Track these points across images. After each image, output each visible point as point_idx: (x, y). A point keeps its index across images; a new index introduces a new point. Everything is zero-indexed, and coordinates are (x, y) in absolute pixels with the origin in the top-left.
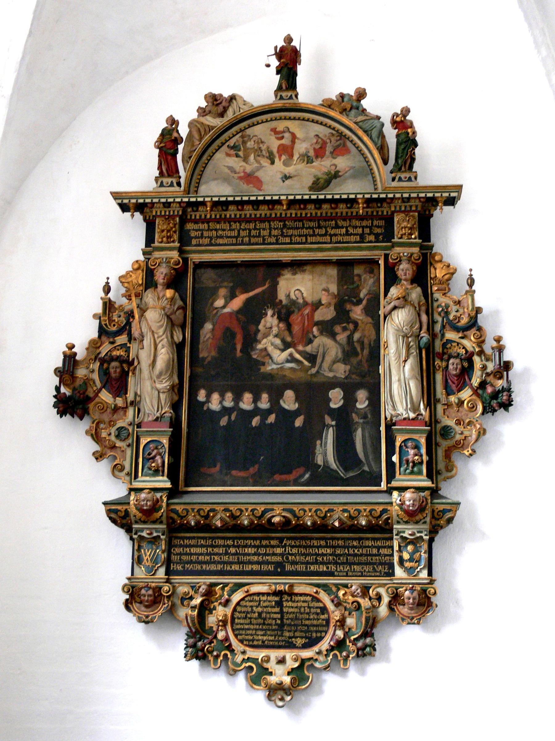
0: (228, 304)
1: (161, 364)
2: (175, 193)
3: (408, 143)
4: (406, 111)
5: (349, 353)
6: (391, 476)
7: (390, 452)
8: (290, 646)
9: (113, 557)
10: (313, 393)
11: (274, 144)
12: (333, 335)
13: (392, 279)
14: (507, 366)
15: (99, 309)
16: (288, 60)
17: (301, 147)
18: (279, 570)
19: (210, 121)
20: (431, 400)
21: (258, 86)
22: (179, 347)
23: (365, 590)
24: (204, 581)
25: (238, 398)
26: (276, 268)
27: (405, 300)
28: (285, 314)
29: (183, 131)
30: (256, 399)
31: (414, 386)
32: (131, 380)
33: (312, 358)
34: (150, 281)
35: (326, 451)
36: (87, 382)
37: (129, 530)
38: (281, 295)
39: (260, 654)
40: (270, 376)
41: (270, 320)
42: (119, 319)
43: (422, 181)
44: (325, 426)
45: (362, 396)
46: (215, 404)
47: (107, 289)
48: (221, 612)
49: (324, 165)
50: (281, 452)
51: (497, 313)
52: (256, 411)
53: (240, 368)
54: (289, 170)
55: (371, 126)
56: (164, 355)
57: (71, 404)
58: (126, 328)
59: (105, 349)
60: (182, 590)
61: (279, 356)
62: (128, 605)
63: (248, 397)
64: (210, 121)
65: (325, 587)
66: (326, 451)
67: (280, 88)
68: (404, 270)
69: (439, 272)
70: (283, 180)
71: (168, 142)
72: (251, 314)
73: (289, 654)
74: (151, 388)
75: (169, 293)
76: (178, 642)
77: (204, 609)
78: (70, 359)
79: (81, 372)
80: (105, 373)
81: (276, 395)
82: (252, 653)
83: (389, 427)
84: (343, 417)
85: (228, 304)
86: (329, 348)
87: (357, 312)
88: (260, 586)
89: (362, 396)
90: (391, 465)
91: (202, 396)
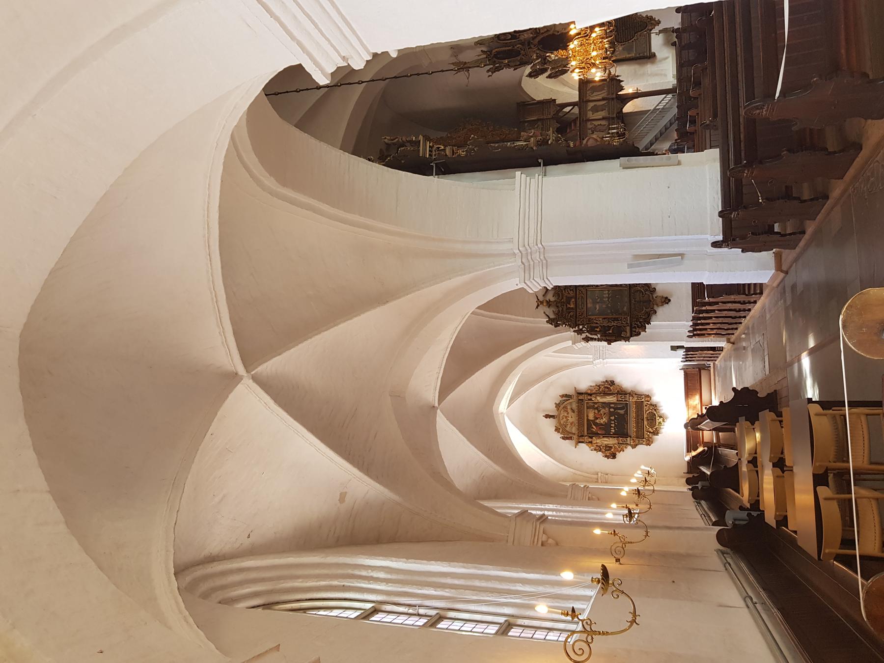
2: (575, 437)
3: (566, 396)
10: (611, 414)
16: (547, 416)
34: (591, 442)
35: (622, 412)
41: (597, 421)
49: (569, 411)
57: (614, 457)
66: (622, 412)
70: (572, 418)
71: (564, 438)
72: (596, 424)
76: (656, 437)
86: (602, 411)
88: (646, 423)
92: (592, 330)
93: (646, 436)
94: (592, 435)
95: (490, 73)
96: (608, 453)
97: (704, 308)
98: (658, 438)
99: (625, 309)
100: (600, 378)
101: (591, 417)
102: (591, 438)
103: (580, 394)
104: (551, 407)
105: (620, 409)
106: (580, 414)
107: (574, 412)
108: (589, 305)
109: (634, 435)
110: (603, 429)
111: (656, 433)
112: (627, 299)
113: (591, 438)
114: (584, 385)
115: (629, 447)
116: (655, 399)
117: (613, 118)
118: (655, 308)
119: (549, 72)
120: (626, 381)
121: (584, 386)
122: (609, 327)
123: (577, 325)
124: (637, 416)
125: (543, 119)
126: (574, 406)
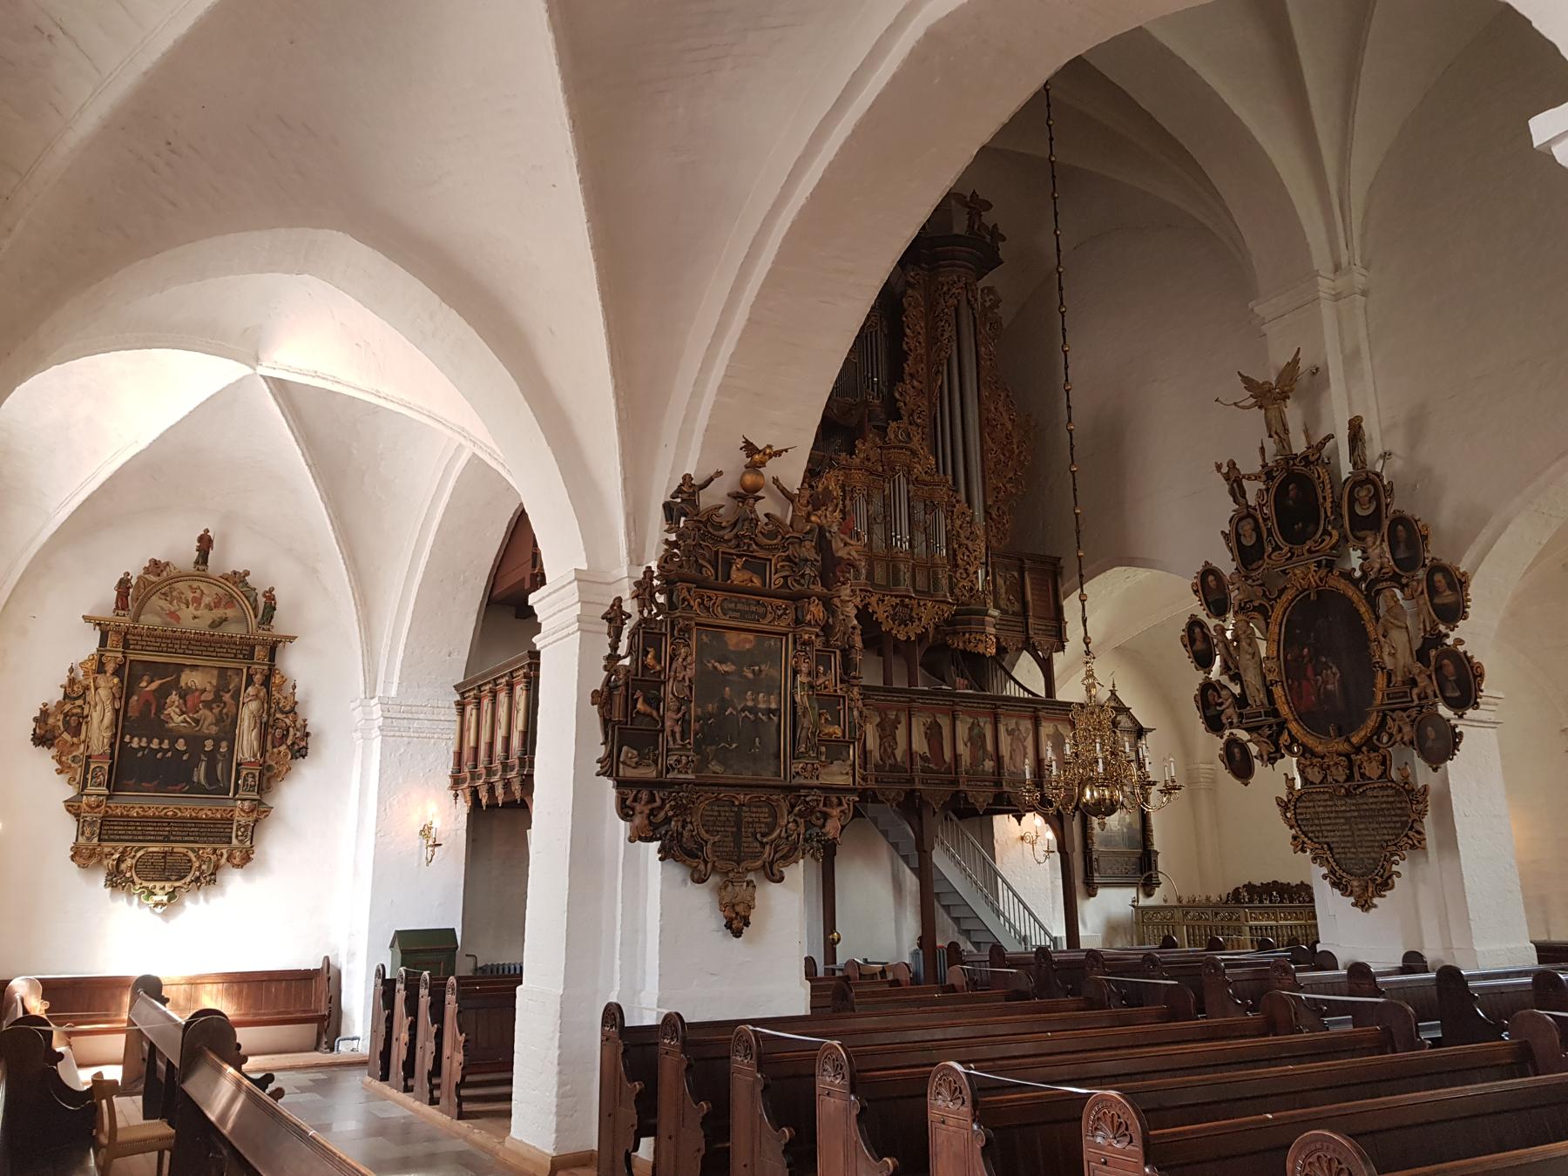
0: (149, 686)
1: (107, 721)
2: (126, 621)
3: (271, 608)
4: (272, 589)
5: (219, 720)
6: (236, 793)
7: (237, 779)
8: (168, 880)
9: (66, 831)
10: (195, 741)
11: (190, 596)
12: (211, 709)
13: (250, 682)
14: (307, 735)
15: (65, 681)
16: (205, 543)
17: (206, 600)
18: (167, 840)
19: (152, 578)
20: (263, 751)
21: (183, 552)
22: (117, 711)
23: (215, 851)
24: (121, 846)
25: (150, 742)
26: (180, 668)
27: (257, 696)
28: (183, 695)
29: (134, 582)
30: (161, 743)
31: (255, 744)
32: (84, 727)
33: (197, 721)
34: (101, 669)
35: (200, 774)
36: (55, 727)
37: (77, 816)
38: (182, 684)
39: (151, 885)
40: (171, 730)
41: (174, 697)
42: (78, 689)
43: (275, 632)
44: (201, 760)
45: (224, 744)
46: (135, 744)
47: (71, 670)
48: (129, 862)
49: (219, 613)
50: (170, 773)
51: (317, 735)
52: (161, 749)
53: (151, 722)
54: (197, 613)
55: (250, 593)
56: (109, 715)
57: (42, 738)
58: (83, 696)
59: (67, 707)
60: (107, 850)
61: (177, 719)
62: (73, 858)
63: (156, 741)
64: (152, 578)
65: (192, 850)
66: (200, 774)
67: (197, 563)
68: (258, 678)
69: (277, 680)
70: (194, 619)
71: (124, 585)
72: (163, 693)
73: (168, 885)
74: (99, 730)
75: (116, 680)
76: (101, 879)
77: (120, 861)
78: (45, 713)
79: (51, 721)
80: (66, 723)
81: (173, 742)
82: (145, 884)
83: (239, 765)
84: (212, 756)
85: (149, 686)
86: (207, 716)
87: (227, 697)
88: (154, 848)
89: (224, 744)
90: (237, 784)
91: (127, 739)
92: (647, 636)
93: (107, 847)
94: (128, 675)
95: (1224, 470)
96: (56, 721)
97: (424, 992)
98: (97, 884)
99: (715, 767)
100: (317, 715)
101: (190, 679)
102: (116, 673)
103: (273, 649)
104: (235, 556)
105: (211, 772)
106: (202, 645)
107: (215, 624)
108: (732, 639)
109: (118, 807)
110: (144, 714)
111: (117, 880)
112: (747, 776)
113: (116, 673)
114: (299, 667)
115: (70, 792)
116: (235, 883)
117: (998, 784)
118: (714, 880)
119: (1212, 623)
120: (297, 795)
121: (297, 666)
122: (654, 702)
123: (669, 586)
124: (181, 823)
125: (1026, 617)
126: (234, 630)
